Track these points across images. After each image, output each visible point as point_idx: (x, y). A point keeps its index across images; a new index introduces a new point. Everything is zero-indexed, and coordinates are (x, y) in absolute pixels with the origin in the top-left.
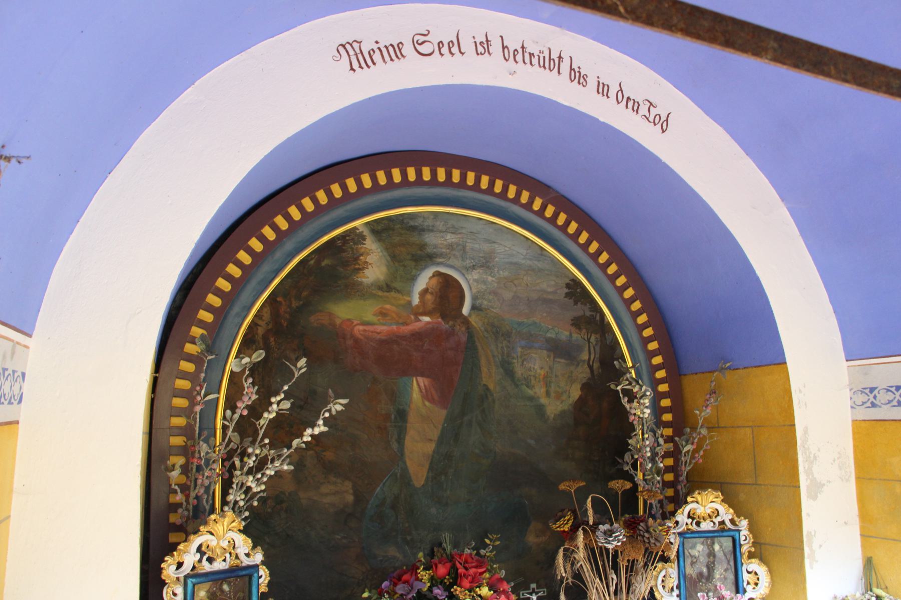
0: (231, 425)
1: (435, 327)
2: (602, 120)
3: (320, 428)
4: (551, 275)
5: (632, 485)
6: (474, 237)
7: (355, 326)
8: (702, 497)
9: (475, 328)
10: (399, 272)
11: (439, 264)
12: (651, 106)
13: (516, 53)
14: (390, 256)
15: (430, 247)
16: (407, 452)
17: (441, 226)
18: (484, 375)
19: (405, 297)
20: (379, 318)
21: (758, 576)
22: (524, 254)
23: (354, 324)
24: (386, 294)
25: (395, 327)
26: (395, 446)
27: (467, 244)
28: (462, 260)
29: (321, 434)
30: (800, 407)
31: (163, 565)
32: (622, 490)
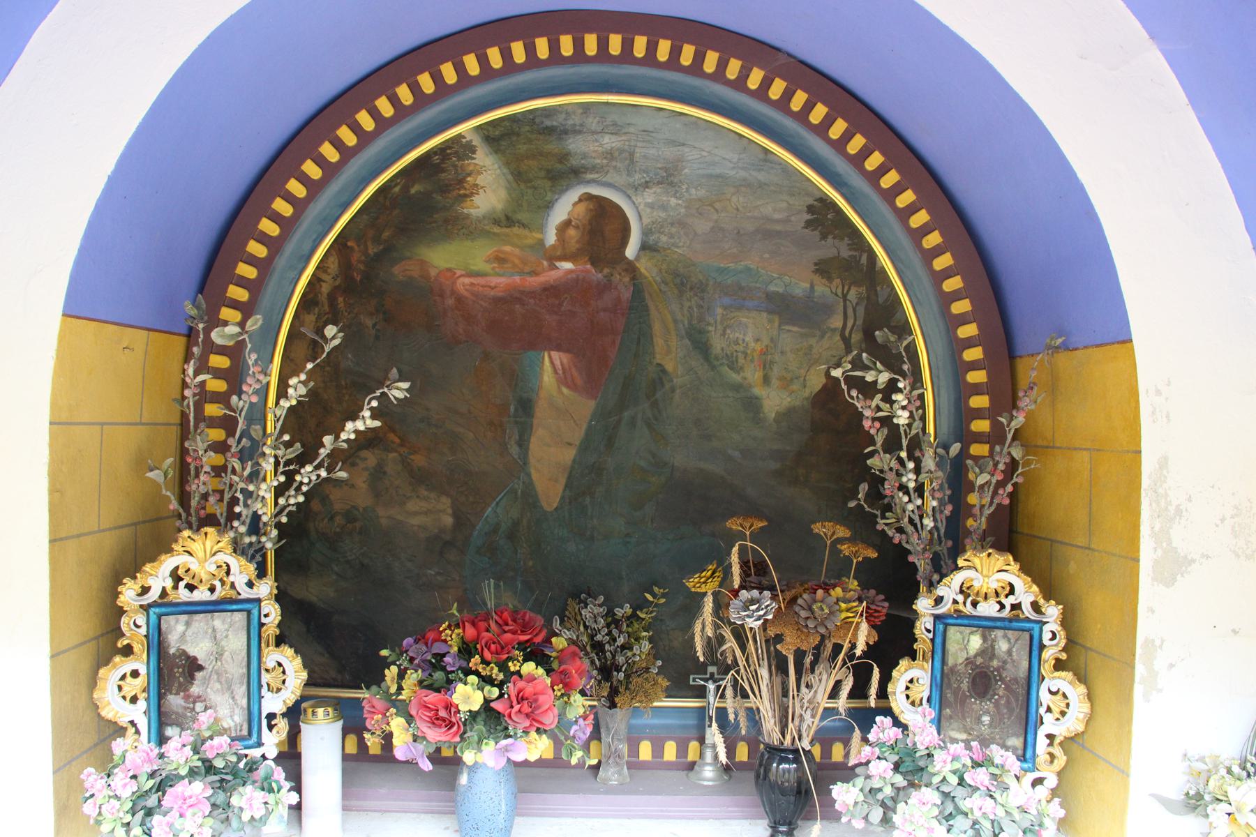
0: (240, 415)
1: (581, 277)
3: (366, 422)
9: (646, 278)
10: (525, 198)
11: (589, 182)
14: (512, 173)
15: (576, 157)
17: (594, 125)
18: (657, 349)
19: (534, 234)
20: (496, 265)
21: (1067, 701)
22: (735, 160)
23: (457, 275)
25: (517, 279)
26: (514, 450)
28: (628, 175)
31: (120, 589)
32: (833, 539)
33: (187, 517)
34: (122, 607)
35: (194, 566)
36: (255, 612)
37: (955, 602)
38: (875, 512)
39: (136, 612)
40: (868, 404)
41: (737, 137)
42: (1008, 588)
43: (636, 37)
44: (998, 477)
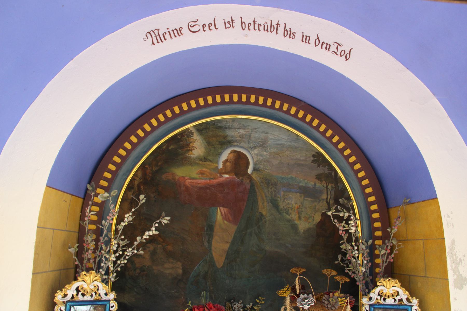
0: (105, 228)
2: (304, 56)
3: (153, 232)
4: (303, 150)
5: (84, 239)
6: (255, 131)
7: (186, 180)
8: (386, 283)
9: (255, 180)
10: (211, 151)
11: (234, 146)
12: (339, 46)
13: (250, 25)
14: (207, 142)
15: (230, 137)
16: (213, 248)
17: (236, 126)
20: (200, 175)
22: (286, 139)
23: (186, 179)
24: (204, 163)
25: (208, 180)
26: (206, 244)
27: (252, 135)
28: (248, 144)
29: (154, 235)
30: (448, 227)
31: (56, 295)
33: (82, 267)
34: (56, 302)
35: (85, 286)
36: (108, 305)
37: (377, 299)
38: (344, 265)
39: (61, 304)
40: (341, 225)
41: (287, 131)
42: (397, 293)
43: (251, 96)
44: (388, 251)
